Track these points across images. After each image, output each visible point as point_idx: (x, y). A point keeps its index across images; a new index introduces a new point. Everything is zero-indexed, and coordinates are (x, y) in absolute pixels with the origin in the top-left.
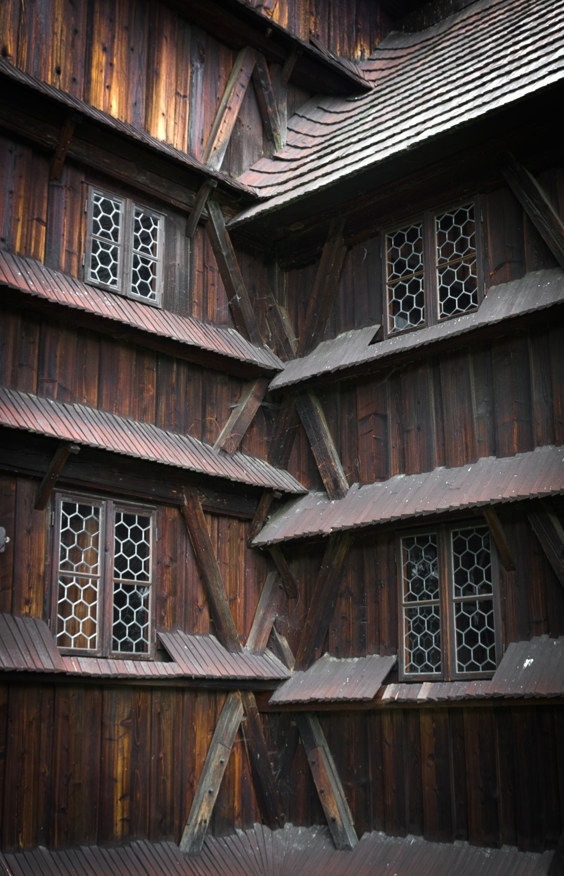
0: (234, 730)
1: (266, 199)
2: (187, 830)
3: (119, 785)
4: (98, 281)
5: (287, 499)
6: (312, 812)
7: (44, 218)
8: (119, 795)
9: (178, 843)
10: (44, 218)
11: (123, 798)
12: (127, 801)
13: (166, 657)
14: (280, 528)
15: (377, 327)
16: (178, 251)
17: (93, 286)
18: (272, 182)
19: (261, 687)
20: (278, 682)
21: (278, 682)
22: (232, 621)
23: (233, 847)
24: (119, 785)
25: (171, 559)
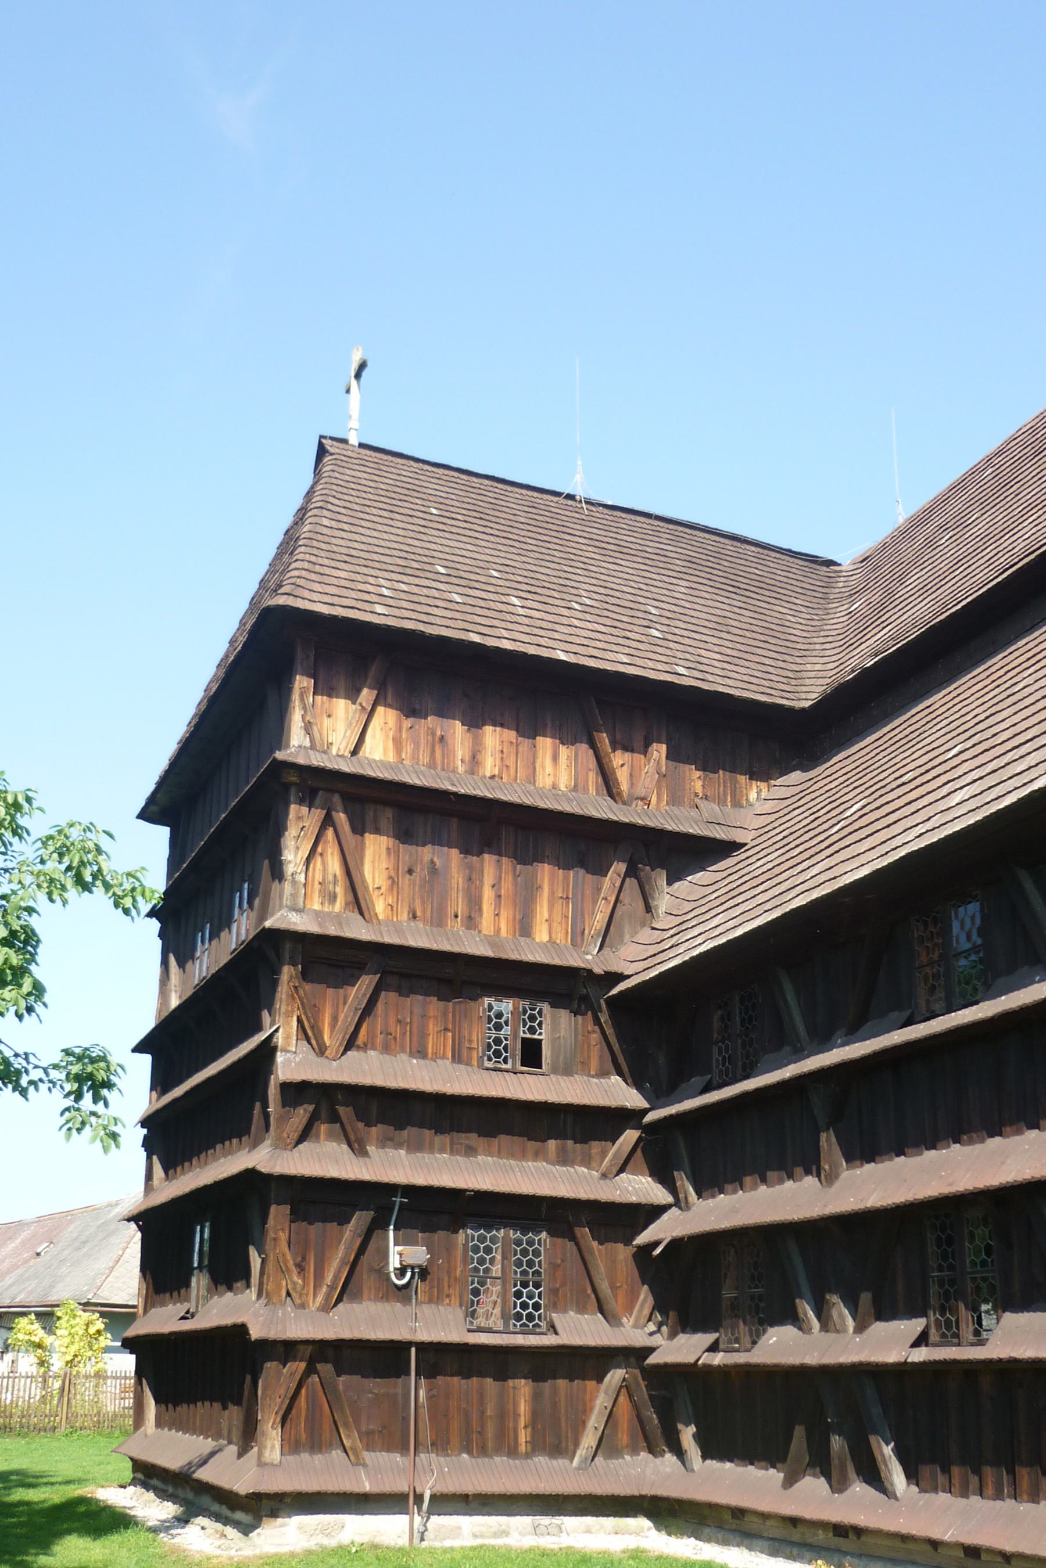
0: (263, 1411)
1: (629, 977)
2: (578, 1453)
3: (522, 1418)
4: (490, 1065)
5: (655, 1211)
6: (679, 1452)
7: (450, 1027)
8: (523, 1425)
9: (572, 1462)
10: (450, 1027)
11: (525, 1427)
12: (529, 1430)
13: (553, 1328)
14: (661, 1231)
15: (709, 1076)
16: (563, 1026)
17: (488, 1069)
18: (641, 956)
19: (635, 1355)
20: (651, 1350)
21: (651, 1350)
22: (615, 1305)
23: (538, 1466)
24: (522, 1418)
25: (562, 1261)
